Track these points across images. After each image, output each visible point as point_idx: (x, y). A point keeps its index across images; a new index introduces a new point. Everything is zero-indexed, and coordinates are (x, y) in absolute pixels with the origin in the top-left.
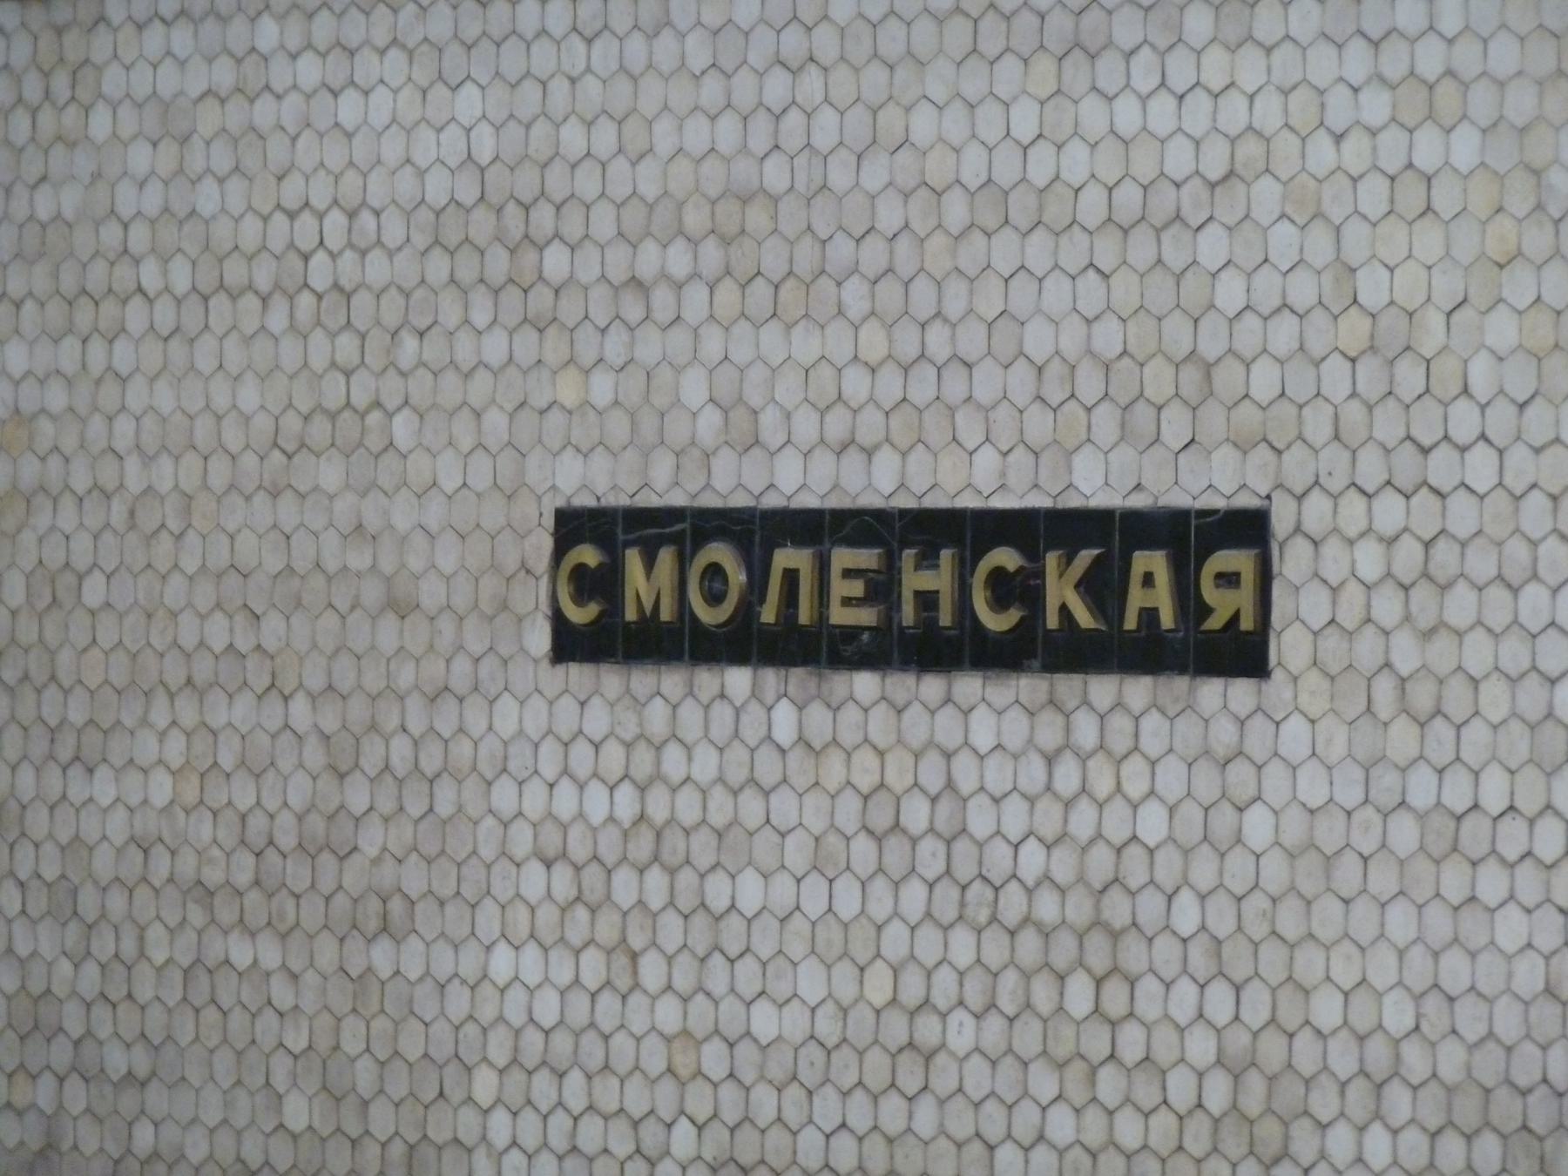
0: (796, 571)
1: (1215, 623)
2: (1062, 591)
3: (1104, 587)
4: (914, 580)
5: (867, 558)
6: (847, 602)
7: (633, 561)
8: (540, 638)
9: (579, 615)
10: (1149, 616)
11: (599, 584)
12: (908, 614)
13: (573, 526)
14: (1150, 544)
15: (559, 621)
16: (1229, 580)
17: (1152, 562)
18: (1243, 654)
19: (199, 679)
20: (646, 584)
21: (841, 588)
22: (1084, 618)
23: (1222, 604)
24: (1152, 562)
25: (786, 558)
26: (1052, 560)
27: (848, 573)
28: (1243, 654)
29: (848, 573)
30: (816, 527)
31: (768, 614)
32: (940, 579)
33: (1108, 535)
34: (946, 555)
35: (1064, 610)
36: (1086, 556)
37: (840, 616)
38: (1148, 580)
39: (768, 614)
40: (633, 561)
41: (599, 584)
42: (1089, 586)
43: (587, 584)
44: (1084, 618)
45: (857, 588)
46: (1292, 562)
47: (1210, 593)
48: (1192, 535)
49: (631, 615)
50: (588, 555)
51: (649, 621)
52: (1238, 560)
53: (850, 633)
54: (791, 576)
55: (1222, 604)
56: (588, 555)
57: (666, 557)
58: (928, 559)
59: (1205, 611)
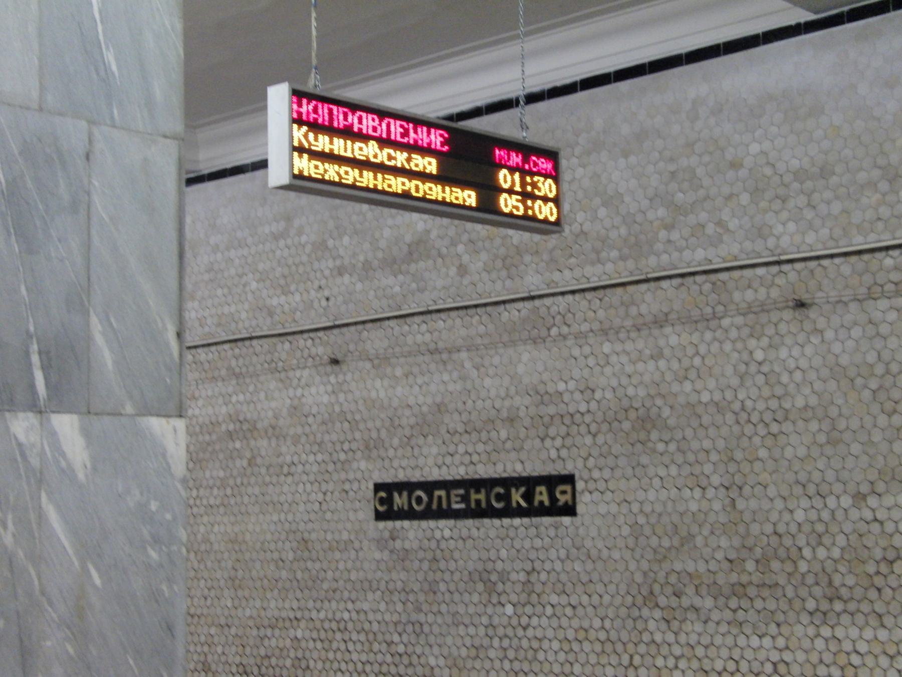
0: (386, 490)
1: (561, 503)
2: (517, 497)
3: (528, 496)
4: (474, 496)
5: (461, 492)
6: (457, 502)
7: (396, 495)
8: (372, 515)
9: (381, 509)
10: (541, 503)
11: (387, 501)
12: (473, 505)
13: (378, 487)
14: (540, 484)
15: (376, 510)
16: (564, 492)
17: (542, 489)
18: (378, 487)
19: (411, 625)
20: (400, 501)
21: (454, 499)
22: (523, 504)
23: (562, 499)
24: (542, 489)
25: (437, 493)
26: (513, 490)
27: (457, 496)
28: (570, 510)
29: (457, 496)
30: (447, 485)
31: (435, 506)
32: (482, 496)
33: (529, 483)
34: (483, 491)
35: (518, 503)
36: (523, 489)
37: (456, 506)
38: (541, 493)
39: (435, 506)
40: (396, 495)
41: (387, 501)
42: (524, 497)
43: (382, 501)
44: (523, 504)
45: (459, 499)
46: (580, 485)
47: (558, 495)
48: (552, 482)
49: (396, 508)
50: (383, 494)
51: (401, 510)
52: (568, 488)
53: (459, 510)
54: (440, 498)
55: (562, 499)
56: (383, 494)
57: (405, 494)
58: (478, 491)
59: (558, 500)
